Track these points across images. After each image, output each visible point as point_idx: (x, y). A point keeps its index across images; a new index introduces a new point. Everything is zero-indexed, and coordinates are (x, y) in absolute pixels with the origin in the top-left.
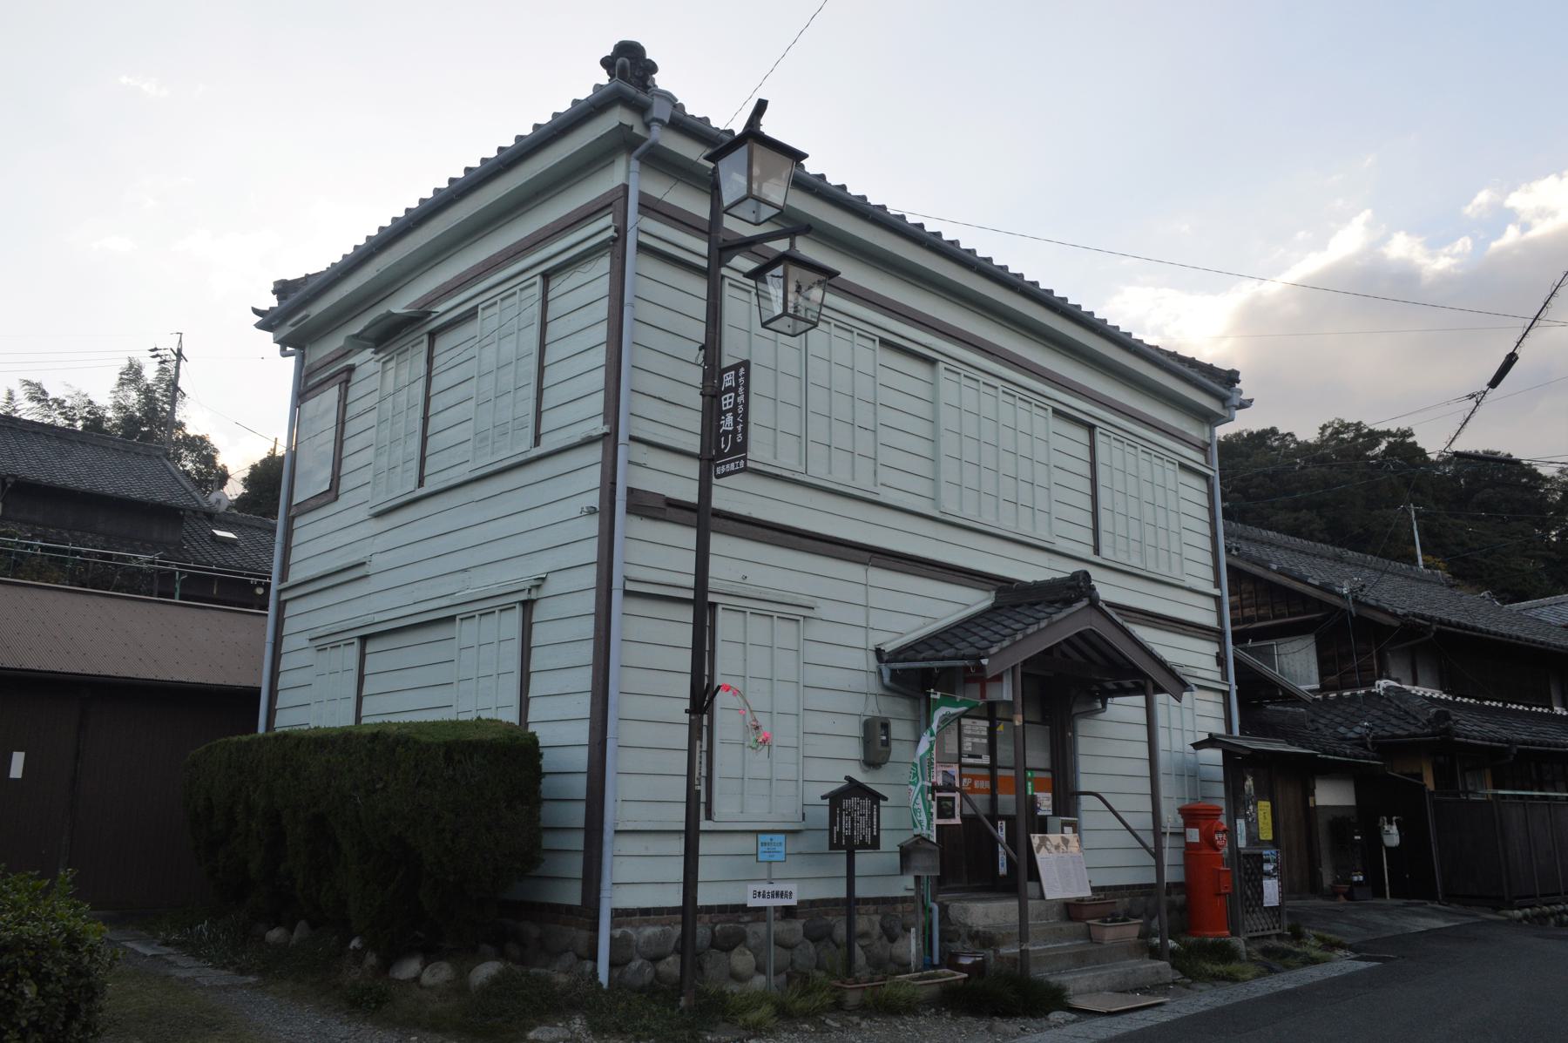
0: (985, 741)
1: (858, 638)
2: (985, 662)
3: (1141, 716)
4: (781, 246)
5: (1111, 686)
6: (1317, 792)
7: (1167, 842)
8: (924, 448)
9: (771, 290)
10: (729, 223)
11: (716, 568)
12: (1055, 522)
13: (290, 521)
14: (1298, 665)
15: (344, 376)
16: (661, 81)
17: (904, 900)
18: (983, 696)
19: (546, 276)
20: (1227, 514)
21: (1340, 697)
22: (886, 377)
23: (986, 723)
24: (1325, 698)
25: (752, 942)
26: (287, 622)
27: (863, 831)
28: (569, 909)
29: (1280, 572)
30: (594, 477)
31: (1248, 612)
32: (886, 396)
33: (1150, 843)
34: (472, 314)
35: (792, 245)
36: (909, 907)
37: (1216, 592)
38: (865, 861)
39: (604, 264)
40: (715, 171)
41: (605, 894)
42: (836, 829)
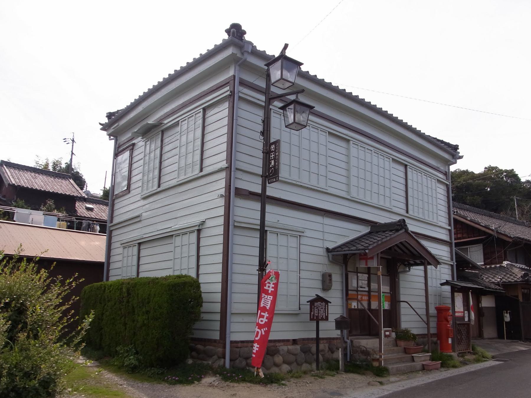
0: (366, 282)
1: (319, 244)
2: (367, 251)
3: (422, 273)
4: (292, 97)
5: (412, 262)
6: (482, 302)
7: (431, 319)
8: (344, 172)
9: (288, 114)
10: (273, 89)
11: (268, 218)
12: (392, 201)
13: (113, 201)
14: (476, 256)
15: (131, 147)
16: (247, 37)
17: (337, 339)
18: (366, 265)
19: (204, 109)
20: (453, 200)
21: (491, 267)
22: (331, 146)
23: (367, 275)
24: (486, 267)
25: (281, 353)
26: (112, 244)
27: (322, 314)
28: (215, 341)
29: (471, 221)
30: (222, 184)
31: (459, 236)
32: (330, 153)
33: (425, 319)
34: (177, 124)
35: (297, 97)
36: (339, 341)
37: (449, 228)
38: (323, 325)
39: (226, 105)
40: (268, 70)
41: (227, 336)
42: (312, 313)
